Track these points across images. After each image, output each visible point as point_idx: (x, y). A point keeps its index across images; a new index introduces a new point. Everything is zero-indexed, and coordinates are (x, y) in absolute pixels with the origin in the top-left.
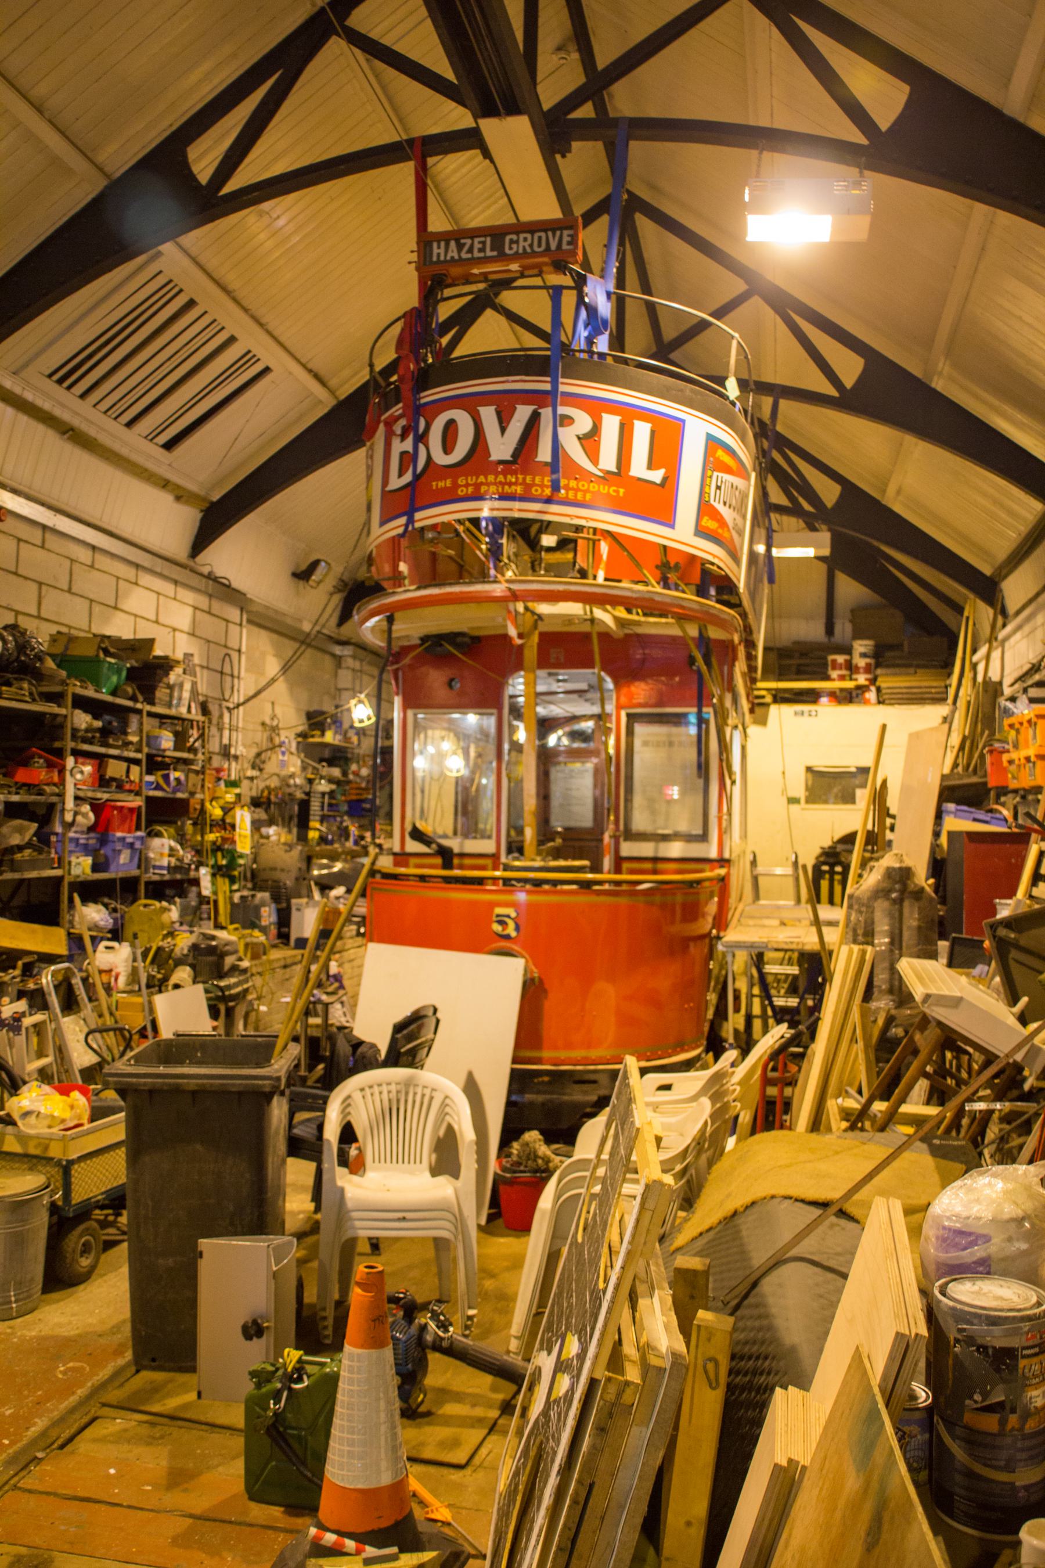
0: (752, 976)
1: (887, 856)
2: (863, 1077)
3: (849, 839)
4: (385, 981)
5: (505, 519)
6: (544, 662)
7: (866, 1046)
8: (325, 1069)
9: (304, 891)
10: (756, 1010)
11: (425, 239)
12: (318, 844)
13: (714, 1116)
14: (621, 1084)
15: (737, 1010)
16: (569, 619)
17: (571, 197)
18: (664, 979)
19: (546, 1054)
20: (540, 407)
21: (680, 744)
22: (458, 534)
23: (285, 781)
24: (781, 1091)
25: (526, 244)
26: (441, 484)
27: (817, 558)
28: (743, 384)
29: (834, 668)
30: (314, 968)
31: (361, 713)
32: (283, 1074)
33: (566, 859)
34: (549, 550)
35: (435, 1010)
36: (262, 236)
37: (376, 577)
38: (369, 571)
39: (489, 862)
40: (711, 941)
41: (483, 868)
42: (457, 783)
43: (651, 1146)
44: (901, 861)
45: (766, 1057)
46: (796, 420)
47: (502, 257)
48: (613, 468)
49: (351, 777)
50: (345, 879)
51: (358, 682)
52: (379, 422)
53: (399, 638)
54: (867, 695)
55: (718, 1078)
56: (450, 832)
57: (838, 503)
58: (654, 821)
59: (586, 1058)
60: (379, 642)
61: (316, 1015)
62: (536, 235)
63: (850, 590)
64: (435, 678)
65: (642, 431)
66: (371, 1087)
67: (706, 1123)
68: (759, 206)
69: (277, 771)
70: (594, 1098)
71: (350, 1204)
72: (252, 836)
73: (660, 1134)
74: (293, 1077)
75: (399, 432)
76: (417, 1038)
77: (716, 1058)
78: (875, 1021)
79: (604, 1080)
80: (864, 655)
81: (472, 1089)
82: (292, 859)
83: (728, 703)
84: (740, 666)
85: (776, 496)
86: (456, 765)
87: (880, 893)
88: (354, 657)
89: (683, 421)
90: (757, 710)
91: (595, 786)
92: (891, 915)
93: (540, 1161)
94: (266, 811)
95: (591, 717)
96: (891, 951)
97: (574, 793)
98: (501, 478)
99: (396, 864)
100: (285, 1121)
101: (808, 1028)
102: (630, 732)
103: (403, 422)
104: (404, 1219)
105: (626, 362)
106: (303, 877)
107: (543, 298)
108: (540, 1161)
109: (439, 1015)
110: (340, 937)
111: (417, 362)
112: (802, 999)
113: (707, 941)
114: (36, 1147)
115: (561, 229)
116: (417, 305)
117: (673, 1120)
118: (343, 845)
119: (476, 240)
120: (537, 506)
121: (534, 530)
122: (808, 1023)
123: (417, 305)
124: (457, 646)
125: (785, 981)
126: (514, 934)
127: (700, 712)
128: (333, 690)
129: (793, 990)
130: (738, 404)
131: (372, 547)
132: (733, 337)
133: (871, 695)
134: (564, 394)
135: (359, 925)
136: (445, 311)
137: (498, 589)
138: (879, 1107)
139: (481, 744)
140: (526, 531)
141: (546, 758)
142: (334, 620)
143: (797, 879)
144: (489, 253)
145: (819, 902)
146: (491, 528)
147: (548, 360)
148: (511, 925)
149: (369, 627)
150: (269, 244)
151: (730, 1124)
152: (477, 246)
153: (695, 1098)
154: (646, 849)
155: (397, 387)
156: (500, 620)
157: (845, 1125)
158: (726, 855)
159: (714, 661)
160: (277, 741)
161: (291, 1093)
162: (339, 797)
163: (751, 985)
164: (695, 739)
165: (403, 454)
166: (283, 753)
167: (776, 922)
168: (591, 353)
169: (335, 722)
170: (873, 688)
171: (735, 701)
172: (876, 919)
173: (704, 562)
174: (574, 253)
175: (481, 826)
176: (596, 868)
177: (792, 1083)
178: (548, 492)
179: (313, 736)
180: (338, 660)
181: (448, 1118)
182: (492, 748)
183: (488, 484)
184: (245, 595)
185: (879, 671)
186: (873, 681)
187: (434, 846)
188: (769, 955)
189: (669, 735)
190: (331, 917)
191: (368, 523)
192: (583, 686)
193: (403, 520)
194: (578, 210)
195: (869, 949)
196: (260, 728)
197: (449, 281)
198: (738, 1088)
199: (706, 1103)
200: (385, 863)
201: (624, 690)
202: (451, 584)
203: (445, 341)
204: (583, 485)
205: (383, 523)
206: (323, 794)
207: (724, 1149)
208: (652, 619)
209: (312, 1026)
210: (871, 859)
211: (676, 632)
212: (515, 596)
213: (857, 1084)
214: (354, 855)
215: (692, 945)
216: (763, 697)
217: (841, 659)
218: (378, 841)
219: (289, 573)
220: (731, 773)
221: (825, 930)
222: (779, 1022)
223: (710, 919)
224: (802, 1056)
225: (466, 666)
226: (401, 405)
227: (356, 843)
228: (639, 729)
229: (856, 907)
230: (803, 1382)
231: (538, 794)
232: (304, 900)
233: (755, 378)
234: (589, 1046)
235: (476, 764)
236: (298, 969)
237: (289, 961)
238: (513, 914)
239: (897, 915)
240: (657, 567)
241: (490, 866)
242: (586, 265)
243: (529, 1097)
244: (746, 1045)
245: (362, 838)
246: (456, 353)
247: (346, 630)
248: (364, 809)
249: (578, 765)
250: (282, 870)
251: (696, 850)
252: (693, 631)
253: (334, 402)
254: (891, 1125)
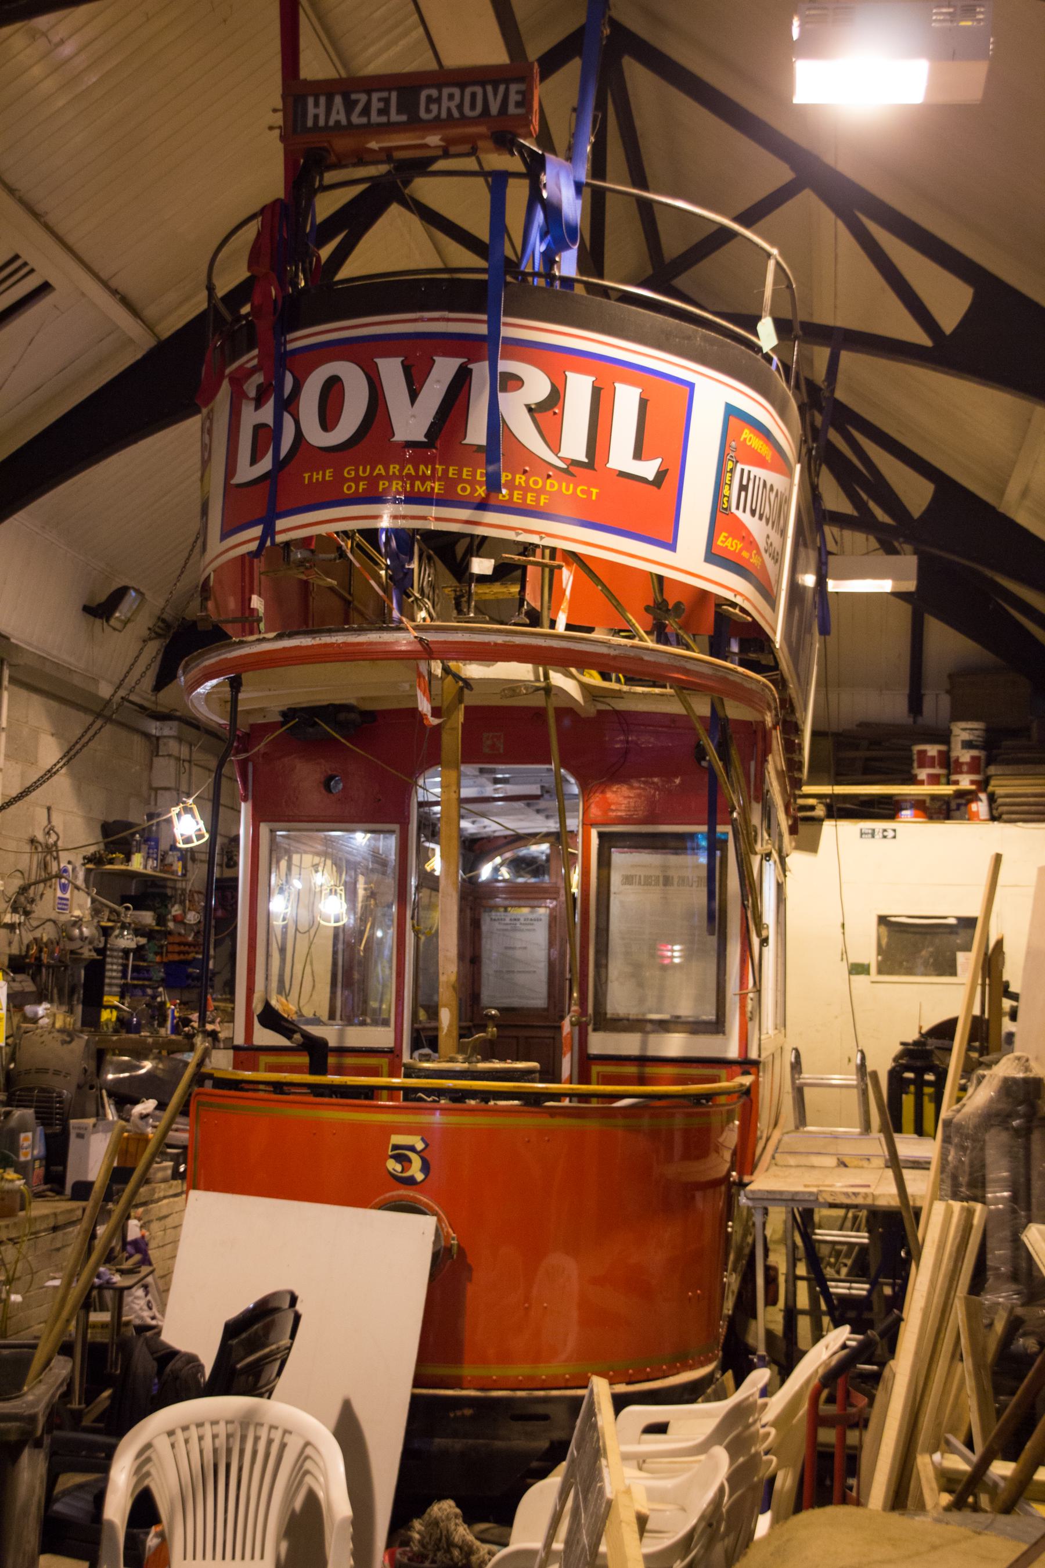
0: (795, 1246)
1: (1004, 1060)
2: (973, 1417)
3: (945, 1030)
4: (217, 1252)
5: (416, 531)
6: (474, 752)
7: (978, 1367)
8: (112, 1397)
9: (91, 1107)
10: (803, 1300)
11: (296, 92)
12: (116, 1031)
13: (735, 1478)
14: (585, 1422)
15: (771, 1300)
16: (511, 687)
17: (522, 28)
18: (655, 1251)
19: (468, 1371)
20: (470, 361)
21: (683, 881)
22: (342, 554)
23: (64, 930)
24: (842, 1437)
25: (453, 105)
26: (317, 476)
27: (894, 594)
28: (782, 327)
29: (922, 765)
30: (101, 1230)
31: (188, 826)
32: (40, 1409)
33: (503, 1059)
34: (482, 579)
35: (294, 1299)
36: (37, 71)
37: (215, 618)
38: (203, 607)
39: (384, 1062)
40: (730, 1189)
41: (375, 1072)
42: (336, 937)
43: (629, 1531)
44: (1027, 1069)
45: (815, 1381)
46: (866, 383)
47: (414, 123)
49: (171, 925)
50: (156, 1087)
51: (184, 778)
52: (221, 377)
53: (248, 712)
54: (974, 807)
55: (741, 1413)
56: (324, 1015)
57: (929, 510)
58: (642, 1000)
59: (531, 1378)
60: (217, 718)
61: (103, 1308)
62: (468, 91)
63: (946, 643)
64: (305, 775)
65: (626, 400)
66: (185, 1428)
67: (721, 1489)
68: (810, 47)
69: (53, 915)
70: (544, 1444)
72: (9, 1018)
73: (644, 1510)
74: (59, 1414)
75: (252, 394)
76: (264, 1346)
77: (738, 1382)
78: (991, 1325)
79: (559, 1413)
80: (968, 745)
81: (349, 1431)
82: (74, 1054)
83: (756, 819)
84: (775, 762)
85: (835, 500)
86: (334, 909)
87: (992, 1118)
88: (180, 739)
89: (691, 386)
90: (802, 828)
91: (551, 944)
92: (1013, 1157)
93: (456, 1552)
94: (33, 979)
95: (546, 837)
96: (1014, 1211)
97: (518, 954)
98: (409, 469)
99: (237, 1065)
100: (39, 1491)
101: (882, 1335)
102: (605, 862)
103: (258, 378)
105: (605, 292)
106: (90, 1083)
107: (479, 190)
108: (456, 1552)
109: (299, 1307)
110: (145, 1180)
111: (282, 287)
112: (874, 1284)
113: (723, 1188)
115: (508, 81)
116: (281, 195)
117: (668, 1484)
118: (155, 1033)
119: (375, 96)
120: (464, 514)
121: (460, 548)
122: (881, 1326)
123: (281, 195)
124: (339, 726)
125: (848, 1256)
126: (420, 1177)
127: (712, 831)
128: (145, 789)
129: (859, 1271)
130: (775, 358)
131: (209, 570)
132: (769, 255)
133: (981, 807)
134: (508, 341)
135: (177, 1160)
136: (326, 206)
137: (403, 640)
138: (1002, 1469)
139: (375, 877)
140: (450, 551)
141: (475, 900)
142: (149, 682)
143: (864, 1093)
144: (394, 117)
145: (899, 1129)
146: (394, 544)
147: (487, 289)
148: (416, 1162)
149: (204, 694)
150: (49, 85)
151: (761, 1492)
153: (703, 1448)
154: (628, 1044)
155: (250, 324)
156: (407, 686)
157: (946, 1498)
158: (753, 1055)
159: (734, 753)
160: (54, 868)
161: (54, 1441)
162: (151, 956)
163: (793, 1262)
164: (704, 873)
165: (258, 428)
166: (64, 888)
167: (831, 1161)
168: (550, 278)
169: (147, 840)
170: (983, 796)
171: (768, 814)
172: (989, 1160)
173: (721, 602)
174: (525, 120)
175: (374, 1004)
176: (551, 1073)
177: (862, 1423)
178: (481, 491)
179: (111, 862)
180: (154, 743)
181: (308, 1479)
182: (390, 883)
183: (390, 478)
184: (7, 638)
185: (992, 770)
186: (983, 785)
187: (297, 1036)
188: (821, 1213)
189: (665, 867)
190: (132, 1149)
191: (202, 534)
192: (535, 790)
193: (257, 531)
194: (535, 51)
195: (978, 1207)
196: (27, 848)
197: (333, 159)
198: (773, 1431)
199: (721, 1455)
200: (221, 1062)
201: (597, 798)
202: (330, 631)
203: (325, 253)
204: (536, 482)
205: (224, 536)
206: (126, 952)
207: (752, 1533)
208: (640, 689)
209: (94, 1326)
210: (980, 1064)
211: (676, 708)
212: (428, 651)
213: (964, 1429)
214: (173, 1049)
215: (699, 1195)
216: (812, 808)
217: (933, 750)
218: (209, 1027)
219: (81, 607)
220: (759, 925)
221: (908, 1174)
222: (837, 1324)
223: (727, 1155)
224: (875, 1378)
225: (350, 759)
226: (256, 352)
227: (175, 1030)
228: (619, 858)
229: (956, 1140)
231: (461, 956)
232: (91, 1121)
233: (802, 316)
234: (537, 1359)
235: (365, 908)
236: (75, 1234)
237: (61, 1220)
238: (420, 1146)
239: (1021, 1153)
240: (647, 609)
241: (385, 1069)
242: (545, 140)
243: (440, 1442)
244: (785, 1358)
245: (186, 1022)
246: (341, 275)
247: (167, 697)
248: (190, 976)
249: (525, 911)
250: (57, 1073)
251: (705, 1046)
252: (702, 708)
253: (152, 343)
254: (1021, 1502)
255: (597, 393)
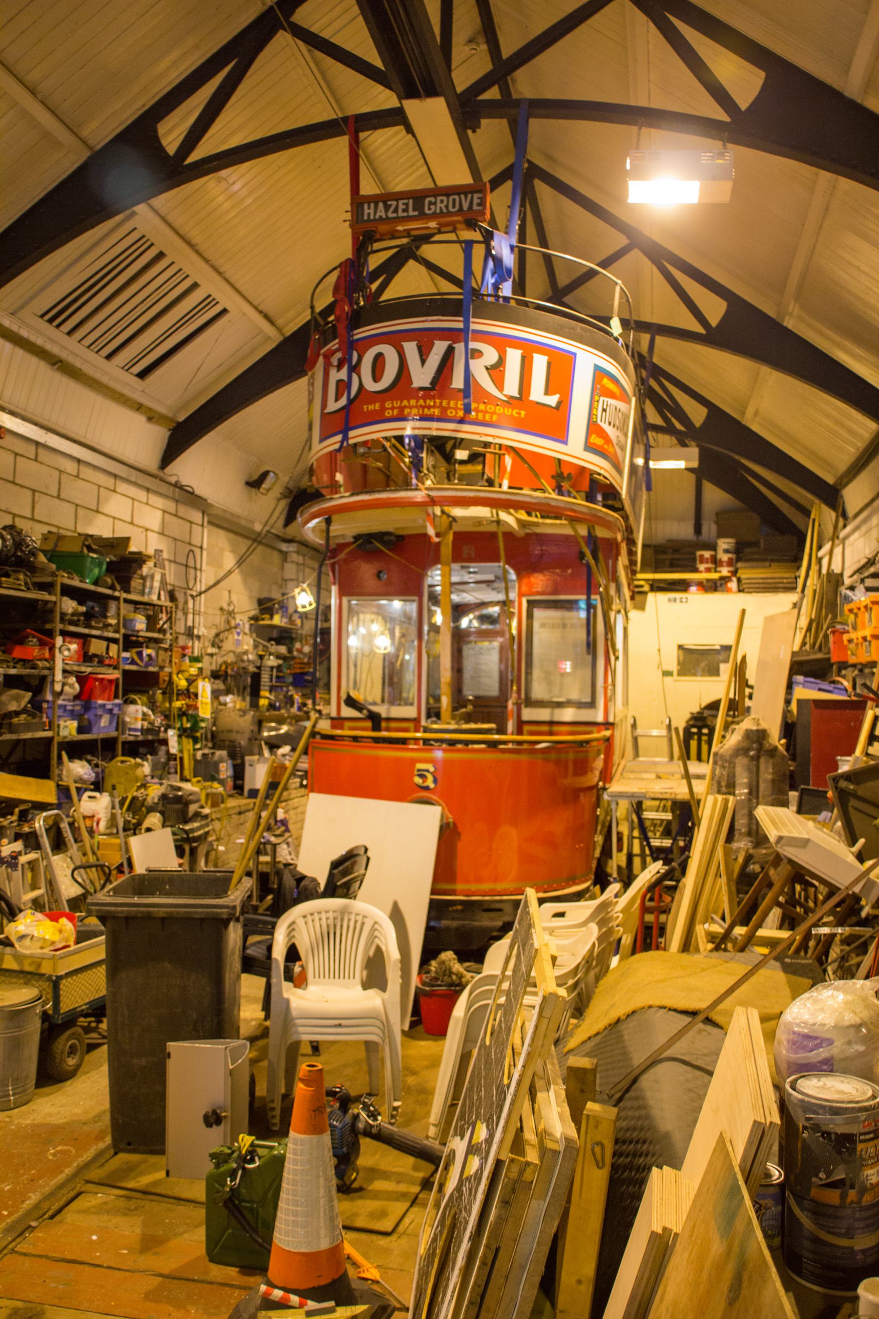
0: (633, 821)
1: (746, 720)
2: (726, 906)
3: (714, 706)
4: (324, 825)
5: (424, 436)
6: (458, 557)
7: (729, 880)
8: (273, 899)
9: (256, 750)
10: (636, 849)
11: (358, 201)
12: (268, 710)
13: (600, 939)
14: (522, 912)
15: (620, 849)
16: (479, 521)
17: (480, 165)
18: (558, 824)
19: (459, 887)
20: (455, 342)
21: (572, 626)
22: (385, 449)
23: (239, 657)
24: (657, 918)
25: (443, 205)
26: (371, 407)
27: (688, 469)
28: (625, 323)
29: (701, 562)
30: (264, 814)
31: (304, 600)
32: (238, 903)
33: (476, 722)
34: (462, 462)
35: (366, 850)
36: (220, 199)
37: (316, 486)
38: (310, 480)
39: (411, 725)
40: (598, 792)
41: (406, 730)
42: (384, 659)
44: (758, 724)
45: (644, 889)
46: (669, 353)
47: (422, 216)
48: (516, 394)
49: (295, 653)
50: (290, 740)
51: (301, 574)
52: (318, 355)
53: (335, 537)
54: (729, 585)
55: (604, 907)
56: (379, 700)
57: (704, 423)
58: (550, 691)
59: (493, 890)
60: (319, 540)
61: (266, 854)
62: (451, 198)
63: (715, 496)
64: (366, 570)
65: (540, 363)
66: (312, 914)
67: (594, 944)
68: (638, 174)
69: (233, 648)
70: (500, 924)
71: (294, 1013)
72: (212, 703)
73: (555, 954)
74: (247, 906)
75: (335, 363)
76: (351, 873)
77: (603, 890)
78: (736, 859)
79: (508, 908)
80: (726, 551)
81: (397, 916)
82: (246, 722)
83: (612, 591)
84: (623, 561)
85: (653, 417)
86: (384, 644)
87: (740, 751)
88: (298, 553)
89: (575, 354)
90: (637, 597)
91: (501, 661)
92: (749, 770)
93: (454, 977)
94: (224, 682)
95: (497, 603)
96: (750, 800)
97: (483, 667)
98: (421, 402)
99: (334, 727)
100: (239, 943)
101: (680, 865)
102: (530, 616)
103: (339, 355)
104: (340, 1025)
105: (526, 304)
106: (255, 738)
107: (457, 251)
108: (454, 977)
109: (369, 854)
110: (286, 788)
111: (351, 305)
112: (675, 840)
113: (595, 791)
114: (30, 965)
115: (472, 193)
116: (350, 256)
117: (566, 942)
118: (288, 711)
119: (401, 202)
120: (452, 426)
121: (449, 446)
122: (680, 861)
123: (350, 256)
124: (384, 543)
125: (660, 825)
126: (432, 786)
127: (588, 599)
128: (280, 580)
129: (667, 833)
130: (621, 340)
131: (313, 460)
132: (616, 284)
133: (733, 585)
134: (474, 331)
135: (302, 778)
136: (374, 262)
137: (419, 496)
138: (740, 931)
139: (405, 626)
140: (442, 447)
141: (459, 638)
142: (281, 522)
143: (670, 740)
144: (411, 213)
145: (689, 758)
146: (413, 444)
147: (461, 303)
148: (430, 778)
149: (311, 527)
150: (227, 205)
151: (614, 946)
152: (401, 207)
153: (584, 924)
154: (543, 714)
155: (334, 326)
156: (421, 521)
157: (710, 946)
158: (611, 720)
159: (601, 556)
160: (233, 623)
161: (245, 919)
162: (285, 670)
163: (632, 829)
164: (585, 622)
165: (339, 382)
166: (238, 634)
167: (653, 776)
168: (497, 297)
169: (281, 607)
170: (734, 579)
171: (618, 589)
172: (737, 773)
173: (592, 473)
174: (483, 213)
175: (405, 695)
176: (501, 730)
177: (666, 911)
178: (461, 414)
179: (263, 619)
180: (284, 555)
181: (376, 940)
182: (413, 629)
183: (410, 407)
184: (206, 500)
185: (739, 565)
186: (734, 573)
187: (365, 712)
188: (647, 804)
189: (563, 618)
190: (278, 772)
191: (309, 440)
192: (491, 577)
193: (339, 438)
194: (487, 177)
195: (731, 798)
196: (219, 612)
197: (378, 236)
198: (621, 915)
199: (594, 928)
200: (324, 726)
201: (525, 581)
202: (379, 491)
203: (374, 287)
204: (490, 408)
205: (322, 440)
206: (272, 668)
207: (609, 966)
208: (548, 521)
209: (262, 863)
210: (733, 723)
211: (569, 531)
212: (433, 502)
213: (721, 912)
214: (298, 719)
215: (582, 795)
216: (642, 586)
217: (707, 554)
218: (318, 708)
219: (243, 482)
220: (615, 650)
221: (694, 782)
222: (655, 860)
223: (597, 773)
224: (674, 888)
225: (392, 560)
226: (337, 341)
227: (299, 709)
228: (538, 613)
229: (720, 763)
230: (676, 1163)
231: (453, 668)
232: (256, 757)
233: (635, 318)
234: (495, 880)
235: (400, 643)
236: (251, 815)
237: (243, 809)
238: (432, 769)
239: (754, 769)
240: (553, 477)
241: (412, 728)
242: (493, 223)
243: (445, 923)
244: (627, 879)
245: (305, 705)
246: (384, 297)
247: (291, 530)
248: (306, 681)
249: (486, 644)
250: (238, 732)
251: (585, 715)
252: (583, 531)
253: (281, 338)
254: (749, 947)
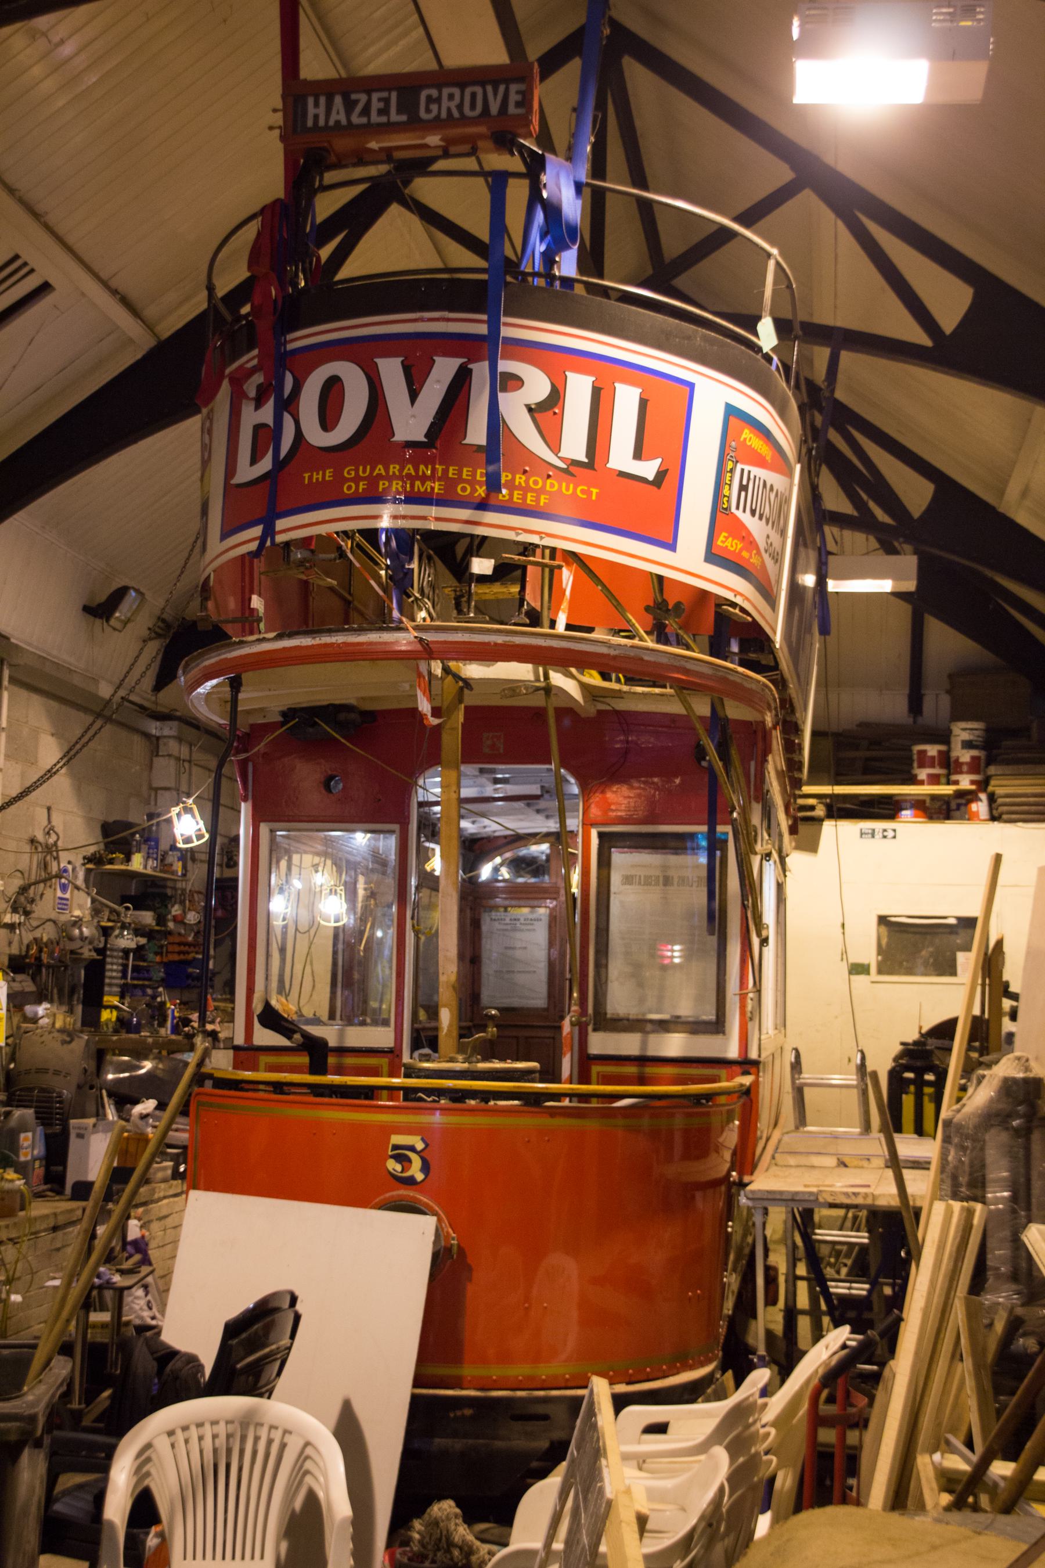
0: (795, 1246)
1: (1004, 1060)
2: (973, 1417)
3: (945, 1030)
4: (217, 1252)
5: (416, 531)
6: (474, 752)
7: (978, 1367)
8: (112, 1397)
9: (91, 1107)
10: (803, 1300)
11: (296, 92)
12: (116, 1031)
13: (735, 1478)
14: (585, 1422)
15: (771, 1300)
16: (511, 687)
17: (522, 28)
18: (655, 1251)
19: (468, 1371)
20: (470, 361)
21: (683, 881)
22: (342, 554)
23: (64, 930)
24: (842, 1437)
25: (453, 105)
26: (317, 476)
27: (894, 594)
28: (782, 327)
29: (922, 765)
30: (101, 1230)
31: (188, 826)
32: (40, 1409)
33: (503, 1059)
34: (482, 579)
35: (294, 1299)
36: (37, 71)
37: (215, 618)
38: (203, 607)
39: (384, 1062)
40: (730, 1189)
41: (375, 1072)
42: (336, 937)
44: (1027, 1069)
45: (815, 1381)
46: (866, 383)
47: (414, 123)
49: (171, 925)
50: (156, 1087)
51: (184, 778)
52: (221, 377)
53: (248, 712)
54: (974, 807)
55: (741, 1413)
56: (324, 1015)
57: (929, 510)
58: (642, 1000)
59: (531, 1378)
60: (217, 718)
61: (103, 1308)
62: (468, 91)
63: (946, 643)
64: (305, 775)
65: (626, 400)
66: (185, 1428)
67: (721, 1489)
68: (810, 47)
69: (53, 915)
70: (544, 1444)
72: (9, 1018)
73: (644, 1510)
74: (59, 1414)
75: (252, 394)
76: (264, 1346)
77: (738, 1382)
78: (991, 1325)
79: (559, 1413)
80: (968, 745)
81: (349, 1431)
82: (74, 1054)
83: (756, 819)
84: (775, 762)
85: (835, 500)
86: (334, 909)
87: (992, 1118)
88: (180, 739)
89: (691, 386)
90: (802, 828)
91: (551, 944)
92: (1013, 1157)
93: (456, 1552)
94: (33, 979)
95: (546, 837)
96: (1014, 1211)
97: (518, 954)
98: (409, 469)
99: (237, 1065)
100: (39, 1491)
101: (882, 1335)
102: (605, 862)
103: (258, 378)
105: (605, 292)
106: (90, 1083)
107: (479, 190)
108: (456, 1552)
109: (299, 1307)
110: (145, 1180)
111: (282, 287)
112: (874, 1284)
113: (723, 1188)
115: (508, 81)
116: (281, 195)
117: (668, 1484)
118: (155, 1033)
119: (375, 96)
120: (464, 514)
121: (460, 548)
122: (881, 1326)
123: (281, 195)
124: (339, 726)
125: (848, 1256)
126: (420, 1177)
127: (712, 831)
128: (145, 789)
129: (859, 1271)
130: (775, 358)
131: (209, 570)
132: (769, 255)
133: (981, 807)
134: (508, 341)
135: (177, 1160)
136: (326, 206)
137: (403, 640)
138: (1002, 1469)
139: (375, 877)
140: (450, 551)
141: (475, 900)
142: (149, 682)
143: (864, 1093)
144: (394, 117)
145: (899, 1129)
146: (394, 544)
147: (487, 289)
148: (416, 1162)
149: (204, 694)
150: (49, 85)
151: (761, 1492)
153: (703, 1448)
154: (628, 1044)
155: (250, 324)
156: (407, 686)
157: (946, 1498)
158: (753, 1055)
159: (734, 753)
160: (54, 868)
161: (54, 1441)
162: (151, 956)
163: (793, 1262)
164: (704, 873)
165: (258, 428)
166: (64, 888)
167: (831, 1161)
168: (550, 278)
169: (147, 840)
170: (983, 796)
171: (768, 814)
172: (989, 1160)
173: (721, 602)
174: (525, 120)
175: (374, 1004)
176: (551, 1073)
177: (862, 1423)
178: (481, 491)
179: (111, 862)
180: (154, 743)
181: (308, 1479)
182: (390, 883)
183: (390, 478)
184: (7, 638)
185: (992, 770)
186: (983, 785)
187: (297, 1036)
188: (821, 1213)
189: (665, 867)
190: (132, 1149)
191: (202, 534)
192: (535, 790)
193: (257, 531)
194: (535, 51)
195: (978, 1207)
196: (27, 848)
197: (333, 159)
198: (773, 1431)
199: (721, 1455)
200: (221, 1062)
201: (597, 798)
202: (330, 631)
203: (325, 253)
204: (536, 482)
205: (224, 536)
206: (126, 952)
207: (752, 1533)
208: (640, 689)
209: (94, 1326)
210: (980, 1064)
211: (676, 708)
212: (428, 651)
213: (964, 1429)
214: (173, 1049)
215: (699, 1195)
216: (812, 808)
217: (933, 750)
218: (209, 1027)
219: (81, 607)
220: (759, 925)
221: (908, 1174)
222: (837, 1324)
223: (727, 1155)
224: (875, 1378)
226: (256, 352)
227: (175, 1030)
228: (619, 858)
229: (956, 1140)
231: (461, 956)
232: (91, 1121)
233: (802, 316)
234: (537, 1359)
235: (365, 908)
236: (75, 1234)
237: (61, 1220)
238: (420, 1146)
239: (1021, 1153)
240: (647, 609)
241: (385, 1069)
242: (545, 140)
243: (440, 1442)
244: (785, 1358)
245: (186, 1022)
246: (341, 275)
247: (167, 697)
248: (190, 976)
249: (525, 911)
250: (57, 1073)
251: (705, 1046)
252: (702, 708)
253: (152, 343)
254: (1021, 1502)
255: (597, 393)
